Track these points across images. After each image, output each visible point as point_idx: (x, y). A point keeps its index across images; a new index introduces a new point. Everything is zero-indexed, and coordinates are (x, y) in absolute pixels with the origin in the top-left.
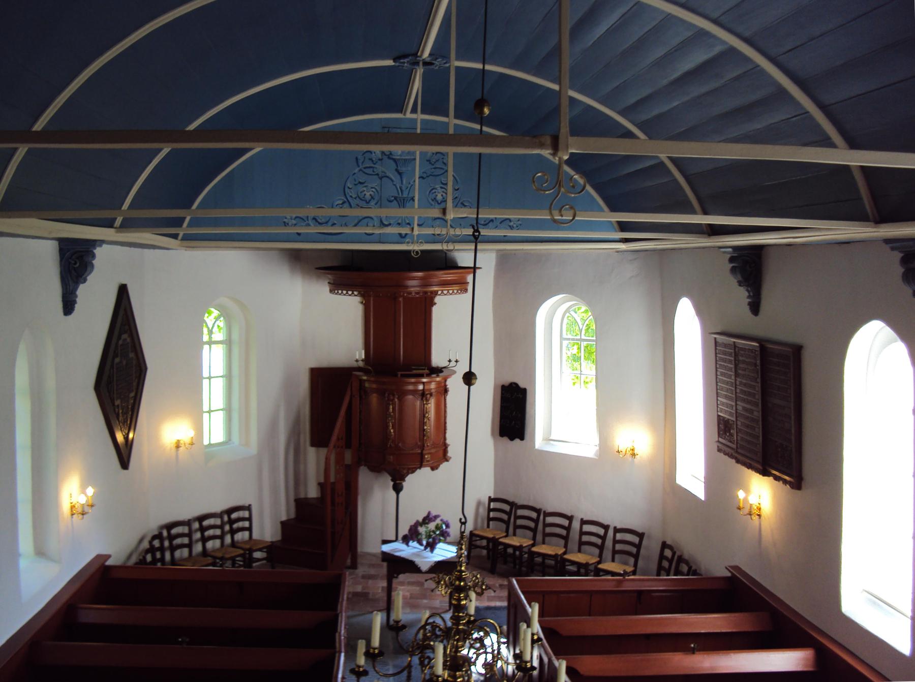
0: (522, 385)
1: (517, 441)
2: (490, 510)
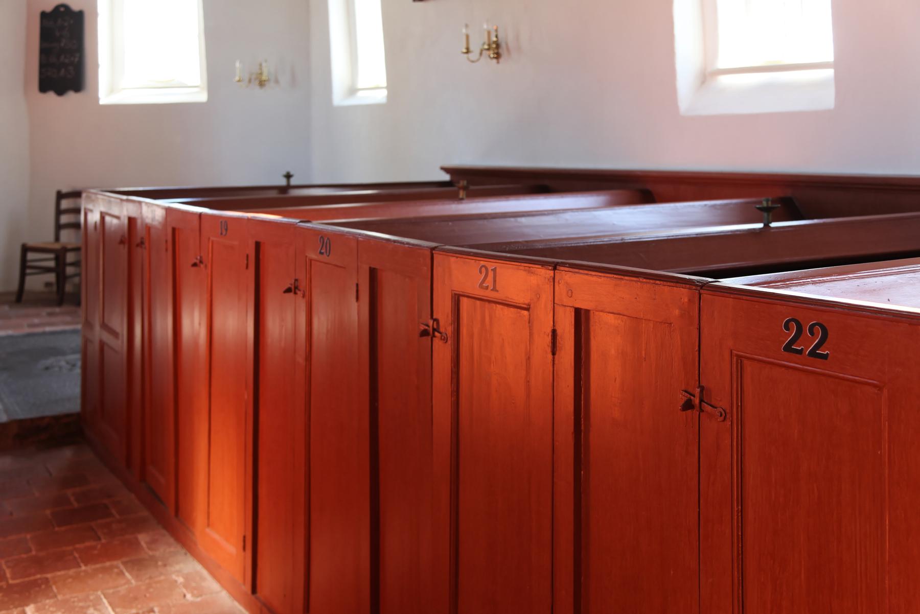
0: (75, 7)
1: (71, 96)
2: (59, 212)
